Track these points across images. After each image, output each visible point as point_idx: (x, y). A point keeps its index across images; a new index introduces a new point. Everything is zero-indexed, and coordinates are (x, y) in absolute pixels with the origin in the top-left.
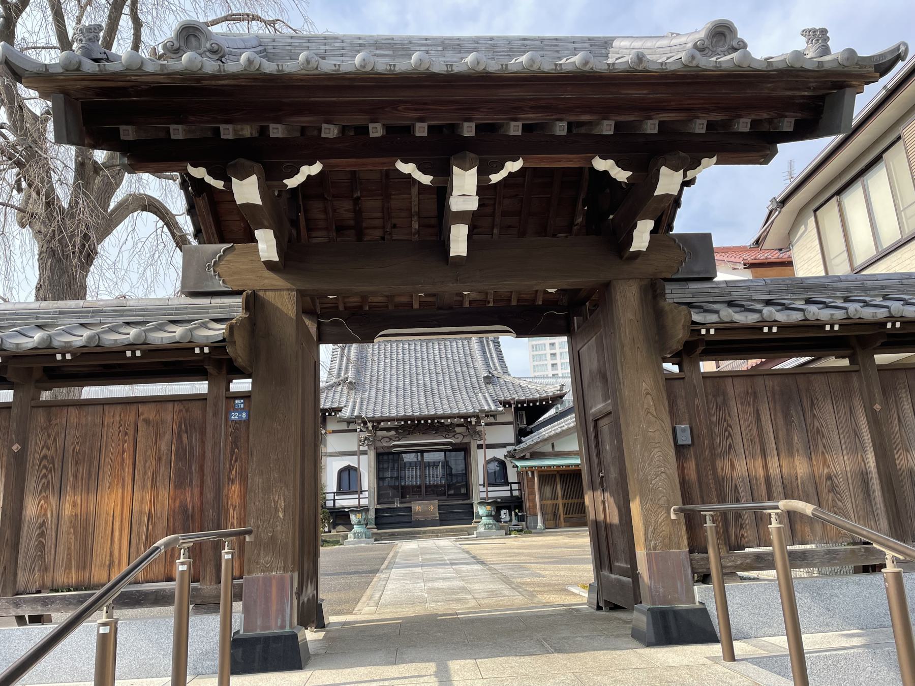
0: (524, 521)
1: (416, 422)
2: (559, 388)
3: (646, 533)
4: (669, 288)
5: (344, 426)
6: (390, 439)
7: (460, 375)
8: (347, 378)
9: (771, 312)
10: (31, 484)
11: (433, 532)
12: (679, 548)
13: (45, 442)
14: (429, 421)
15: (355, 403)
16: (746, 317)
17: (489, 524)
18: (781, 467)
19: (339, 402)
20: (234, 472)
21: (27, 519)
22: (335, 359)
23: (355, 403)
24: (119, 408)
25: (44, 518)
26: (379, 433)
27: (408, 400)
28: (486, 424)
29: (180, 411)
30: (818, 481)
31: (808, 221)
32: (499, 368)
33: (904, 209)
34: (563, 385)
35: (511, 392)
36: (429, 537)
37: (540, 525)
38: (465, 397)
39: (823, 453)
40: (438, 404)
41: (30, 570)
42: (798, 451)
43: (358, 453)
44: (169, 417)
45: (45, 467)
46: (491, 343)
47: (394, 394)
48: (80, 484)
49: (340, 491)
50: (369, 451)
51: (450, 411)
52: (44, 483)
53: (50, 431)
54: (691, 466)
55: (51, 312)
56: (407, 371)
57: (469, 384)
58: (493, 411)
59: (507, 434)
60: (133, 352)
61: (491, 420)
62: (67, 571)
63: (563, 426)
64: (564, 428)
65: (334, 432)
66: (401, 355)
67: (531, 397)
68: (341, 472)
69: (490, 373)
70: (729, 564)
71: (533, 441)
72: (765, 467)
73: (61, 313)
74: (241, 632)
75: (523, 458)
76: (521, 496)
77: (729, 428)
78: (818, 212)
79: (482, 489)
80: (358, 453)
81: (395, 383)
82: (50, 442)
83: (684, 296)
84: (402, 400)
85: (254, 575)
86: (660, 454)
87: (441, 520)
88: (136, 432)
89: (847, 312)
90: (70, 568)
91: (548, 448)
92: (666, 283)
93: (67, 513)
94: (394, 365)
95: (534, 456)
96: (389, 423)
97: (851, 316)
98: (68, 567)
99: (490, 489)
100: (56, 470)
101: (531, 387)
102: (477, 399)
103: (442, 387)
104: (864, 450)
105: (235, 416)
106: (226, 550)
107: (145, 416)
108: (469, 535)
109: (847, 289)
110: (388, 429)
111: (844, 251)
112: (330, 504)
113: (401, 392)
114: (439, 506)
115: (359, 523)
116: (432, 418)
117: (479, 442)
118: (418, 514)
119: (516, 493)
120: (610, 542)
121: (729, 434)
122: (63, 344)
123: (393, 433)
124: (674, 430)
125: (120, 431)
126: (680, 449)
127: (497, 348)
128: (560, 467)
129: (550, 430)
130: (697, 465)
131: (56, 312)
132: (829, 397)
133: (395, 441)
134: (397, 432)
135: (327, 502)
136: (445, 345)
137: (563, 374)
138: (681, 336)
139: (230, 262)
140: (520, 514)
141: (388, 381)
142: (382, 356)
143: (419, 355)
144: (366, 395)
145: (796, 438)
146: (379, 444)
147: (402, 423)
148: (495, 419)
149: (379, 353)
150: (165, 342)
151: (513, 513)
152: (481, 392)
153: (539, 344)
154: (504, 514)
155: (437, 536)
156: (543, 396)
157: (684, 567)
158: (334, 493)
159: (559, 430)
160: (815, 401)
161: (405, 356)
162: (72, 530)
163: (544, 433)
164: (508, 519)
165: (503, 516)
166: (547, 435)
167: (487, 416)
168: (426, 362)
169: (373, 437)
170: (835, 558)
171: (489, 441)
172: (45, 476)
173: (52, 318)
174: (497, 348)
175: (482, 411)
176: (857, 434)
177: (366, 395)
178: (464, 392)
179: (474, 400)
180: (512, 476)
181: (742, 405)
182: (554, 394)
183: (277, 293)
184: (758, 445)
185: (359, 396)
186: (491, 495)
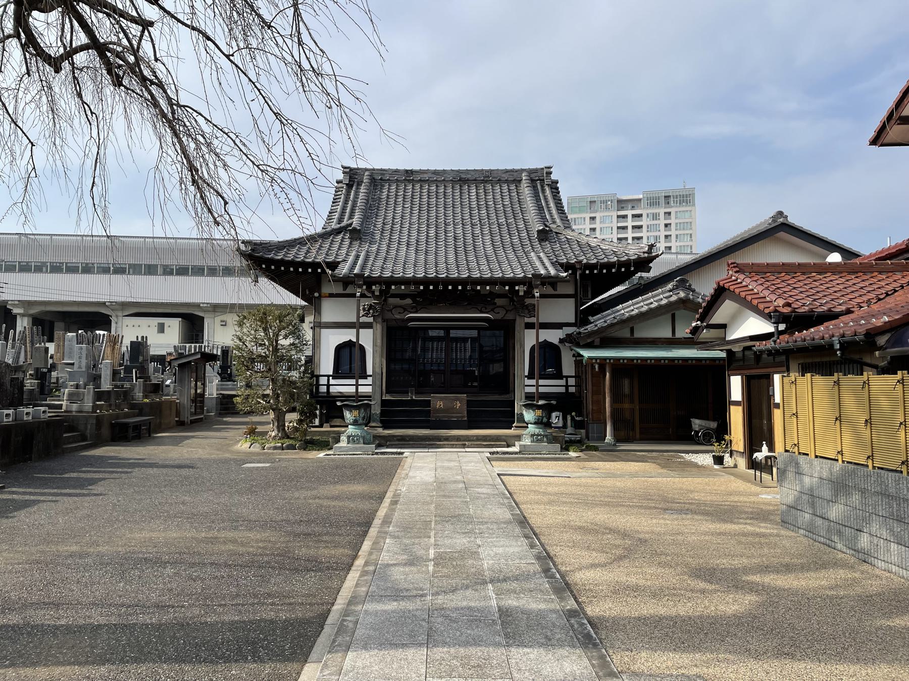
0: (583, 428)
1: (441, 288)
5: (338, 289)
6: (405, 310)
7: (504, 228)
8: (351, 224)
11: (458, 438)
14: (460, 288)
15: (357, 257)
17: (538, 435)
19: (337, 255)
22: (339, 200)
23: (357, 257)
26: (392, 301)
27: (431, 258)
28: (542, 296)
32: (558, 221)
35: (577, 253)
36: (452, 446)
37: (609, 438)
38: (512, 256)
40: (473, 265)
43: (357, 325)
46: (547, 188)
47: (413, 248)
49: (338, 373)
50: (374, 324)
51: (490, 275)
56: (433, 220)
57: (516, 240)
58: (552, 277)
59: (565, 311)
61: (549, 290)
63: (652, 303)
64: (652, 306)
65: (331, 295)
66: (425, 199)
67: (606, 260)
68: (339, 349)
69: (546, 226)
71: (605, 322)
75: (590, 346)
76: (580, 393)
79: (528, 382)
80: (357, 325)
81: (414, 233)
84: (423, 257)
87: (469, 421)
91: (626, 334)
94: (416, 212)
95: (606, 340)
96: (403, 287)
99: (541, 382)
102: (529, 260)
103: (479, 243)
108: (508, 446)
110: (403, 296)
112: (323, 389)
113: (423, 247)
114: (468, 401)
115: (355, 423)
116: (464, 282)
117: (527, 320)
118: (439, 410)
119: (572, 390)
123: (408, 301)
127: (556, 196)
129: (632, 308)
133: (411, 313)
134: (414, 301)
135: (320, 387)
136: (485, 190)
140: (577, 419)
141: (406, 231)
142: (400, 199)
143: (450, 200)
144: (374, 248)
146: (388, 315)
147: (422, 288)
148: (555, 289)
149: (396, 195)
151: (569, 418)
152: (534, 251)
153: (578, 218)
154: (556, 418)
155: (464, 446)
158: (328, 376)
159: (645, 308)
161: (431, 200)
163: (623, 312)
164: (560, 424)
165: (554, 420)
167: (543, 284)
168: (458, 210)
169: (380, 306)
171: (543, 319)
174: (556, 196)
175: (537, 276)
177: (374, 248)
178: (510, 251)
179: (524, 261)
180: (568, 368)
185: (366, 247)
186: (541, 390)
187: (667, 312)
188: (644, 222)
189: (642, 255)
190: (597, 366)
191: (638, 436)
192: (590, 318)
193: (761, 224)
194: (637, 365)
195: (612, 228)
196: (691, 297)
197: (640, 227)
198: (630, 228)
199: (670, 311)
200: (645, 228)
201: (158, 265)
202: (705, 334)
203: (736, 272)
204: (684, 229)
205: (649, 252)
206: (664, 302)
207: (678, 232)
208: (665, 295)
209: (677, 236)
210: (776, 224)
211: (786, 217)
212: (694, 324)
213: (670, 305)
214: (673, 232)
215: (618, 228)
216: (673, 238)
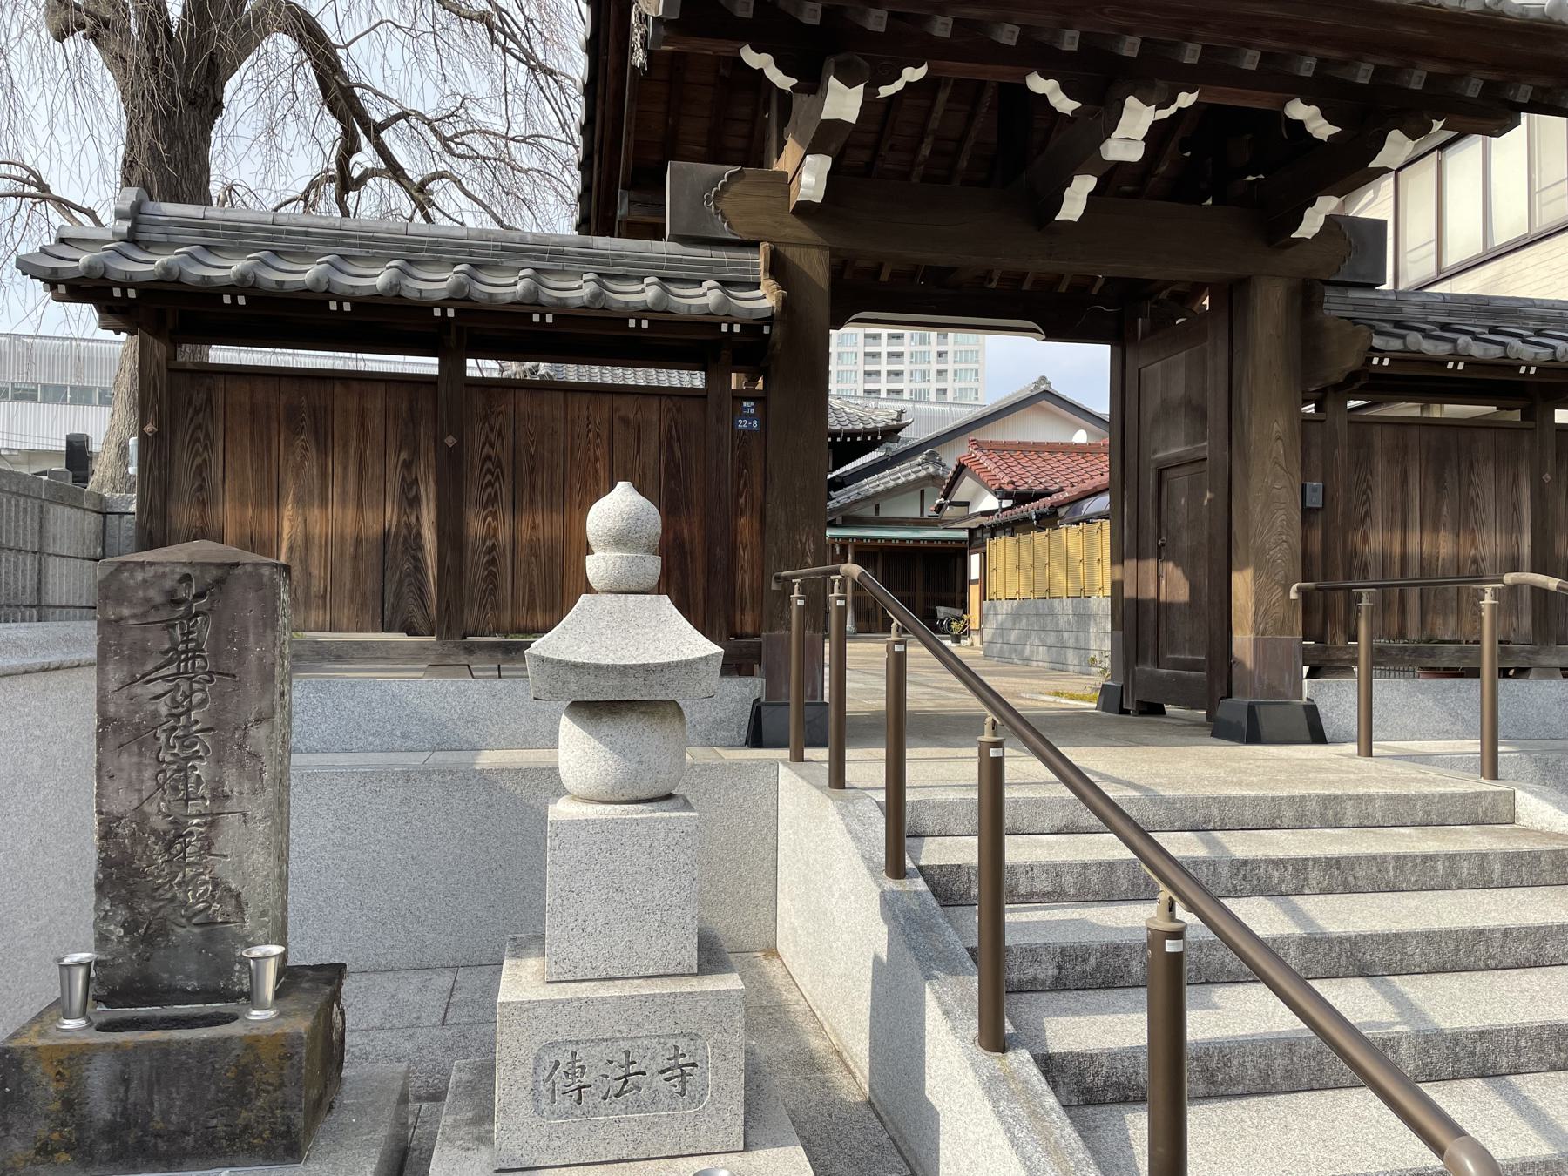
2: (895, 416)
3: (1256, 614)
4: (1330, 293)
9: (1468, 344)
10: (473, 492)
12: (1292, 633)
13: (487, 437)
16: (1436, 346)
18: (1422, 544)
20: (742, 500)
21: (471, 539)
24: (585, 398)
25: (493, 540)
29: (669, 410)
30: (1461, 565)
31: (1383, 184)
33: (1539, 191)
34: (902, 412)
39: (1473, 531)
41: (480, 606)
42: (1444, 525)
44: (655, 418)
45: (489, 471)
48: (539, 498)
52: (490, 494)
53: (492, 422)
54: (1316, 536)
55: (489, 246)
60: (234, 299)
62: (530, 612)
64: (899, 481)
67: (850, 427)
70: (1347, 657)
72: (1404, 543)
73: (504, 249)
74: (763, 700)
77: (1368, 491)
78: (1400, 173)
82: (492, 437)
83: (1343, 307)
85: (777, 632)
86: (1284, 517)
88: (611, 433)
89: (1554, 353)
90: (534, 608)
91: (869, 512)
92: (1326, 288)
93: (524, 536)
97: (1559, 358)
98: (531, 607)
100: (505, 476)
101: (848, 411)
104: (1520, 531)
105: (742, 424)
106: (796, 595)
107: (622, 413)
109: (1542, 319)
111: (1431, 242)
120: (1163, 628)
121: (1368, 497)
122: (555, 301)
124: (1304, 488)
125: (589, 431)
126: (1307, 513)
128: (905, 541)
130: (1325, 535)
131: (497, 246)
132: (1492, 465)
137: (838, 390)
138: (1350, 364)
139: (736, 195)
145: (1445, 509)
150: (694, 311)
156: (869, 426)
157: (1295, 657)
159: (892, 484)
160: (1475, 464)
162: (533, 558)
166: (872, 490)
170: (1466, 657)
172: (490, 484)
173: (494, 256)
176: (1516, 509)
181: (1388, 461)
182: (887, 426)
183: (804, 250)
184: (1399, 515)
187: (916, 488)
188: (904, 366)
189: (891, 423)
190: (838, 549)
191: (880, 628)
192: (832, 493)
193: (1022, 391)
194: (882, 548)
195: (856, 372)
196: (941, 473)
197: (900, 355)
198: (884, 375)
199: (919, 487)
200: (907, 357)
201: (66, 387)
202: (949, 512)
203: (976, 449)
204: (966, 362)
205: (898, 419)
206: (912, 477)
207: (958, 367)
208: (914, 470)
209: (955, 372)
210: (1039, 391)
211: (1050, 383)
212: (937, 501)
213: (918, 481)
214: (950, 366)
215: (866, 354)
216: (950, 375)
